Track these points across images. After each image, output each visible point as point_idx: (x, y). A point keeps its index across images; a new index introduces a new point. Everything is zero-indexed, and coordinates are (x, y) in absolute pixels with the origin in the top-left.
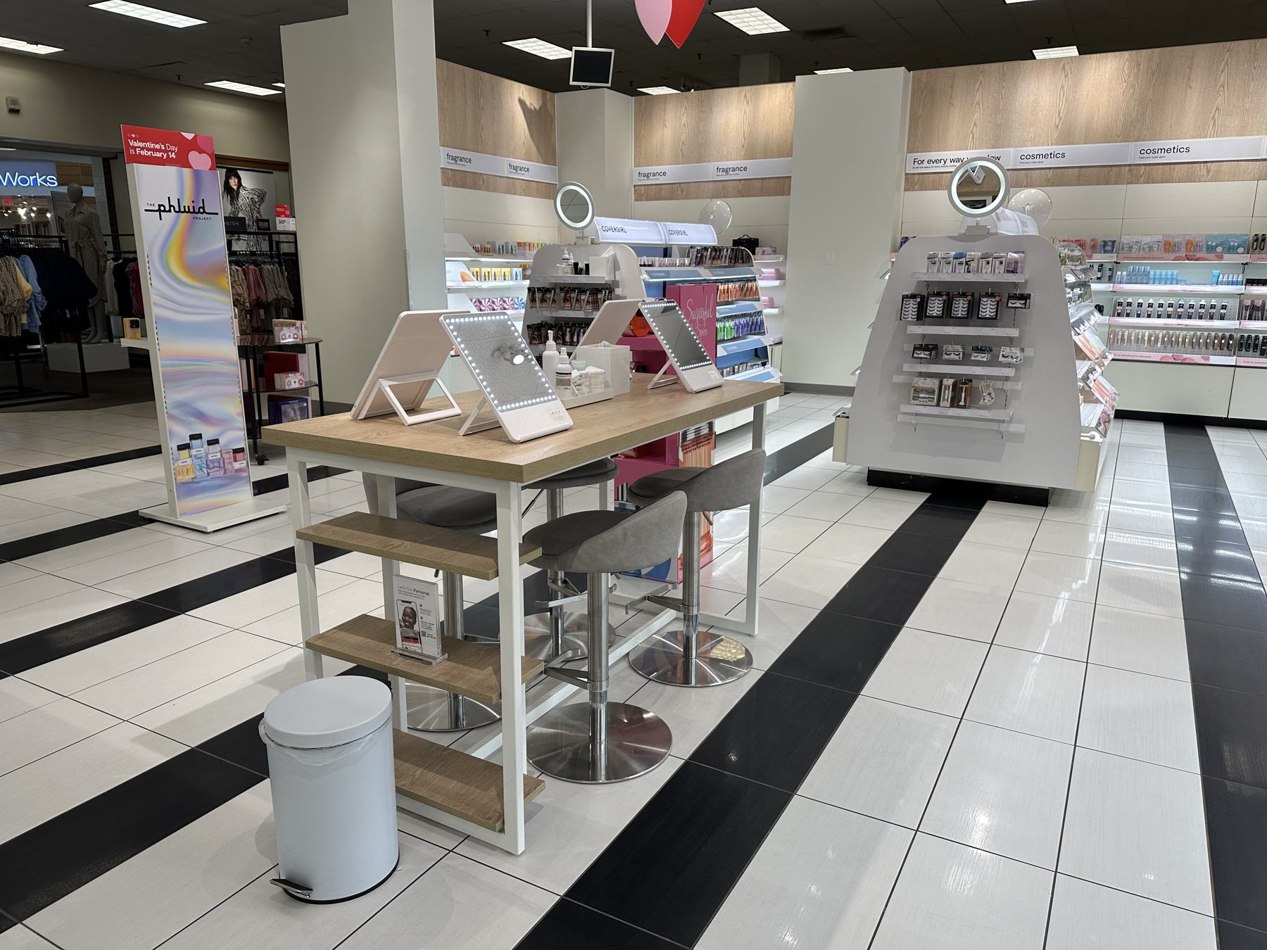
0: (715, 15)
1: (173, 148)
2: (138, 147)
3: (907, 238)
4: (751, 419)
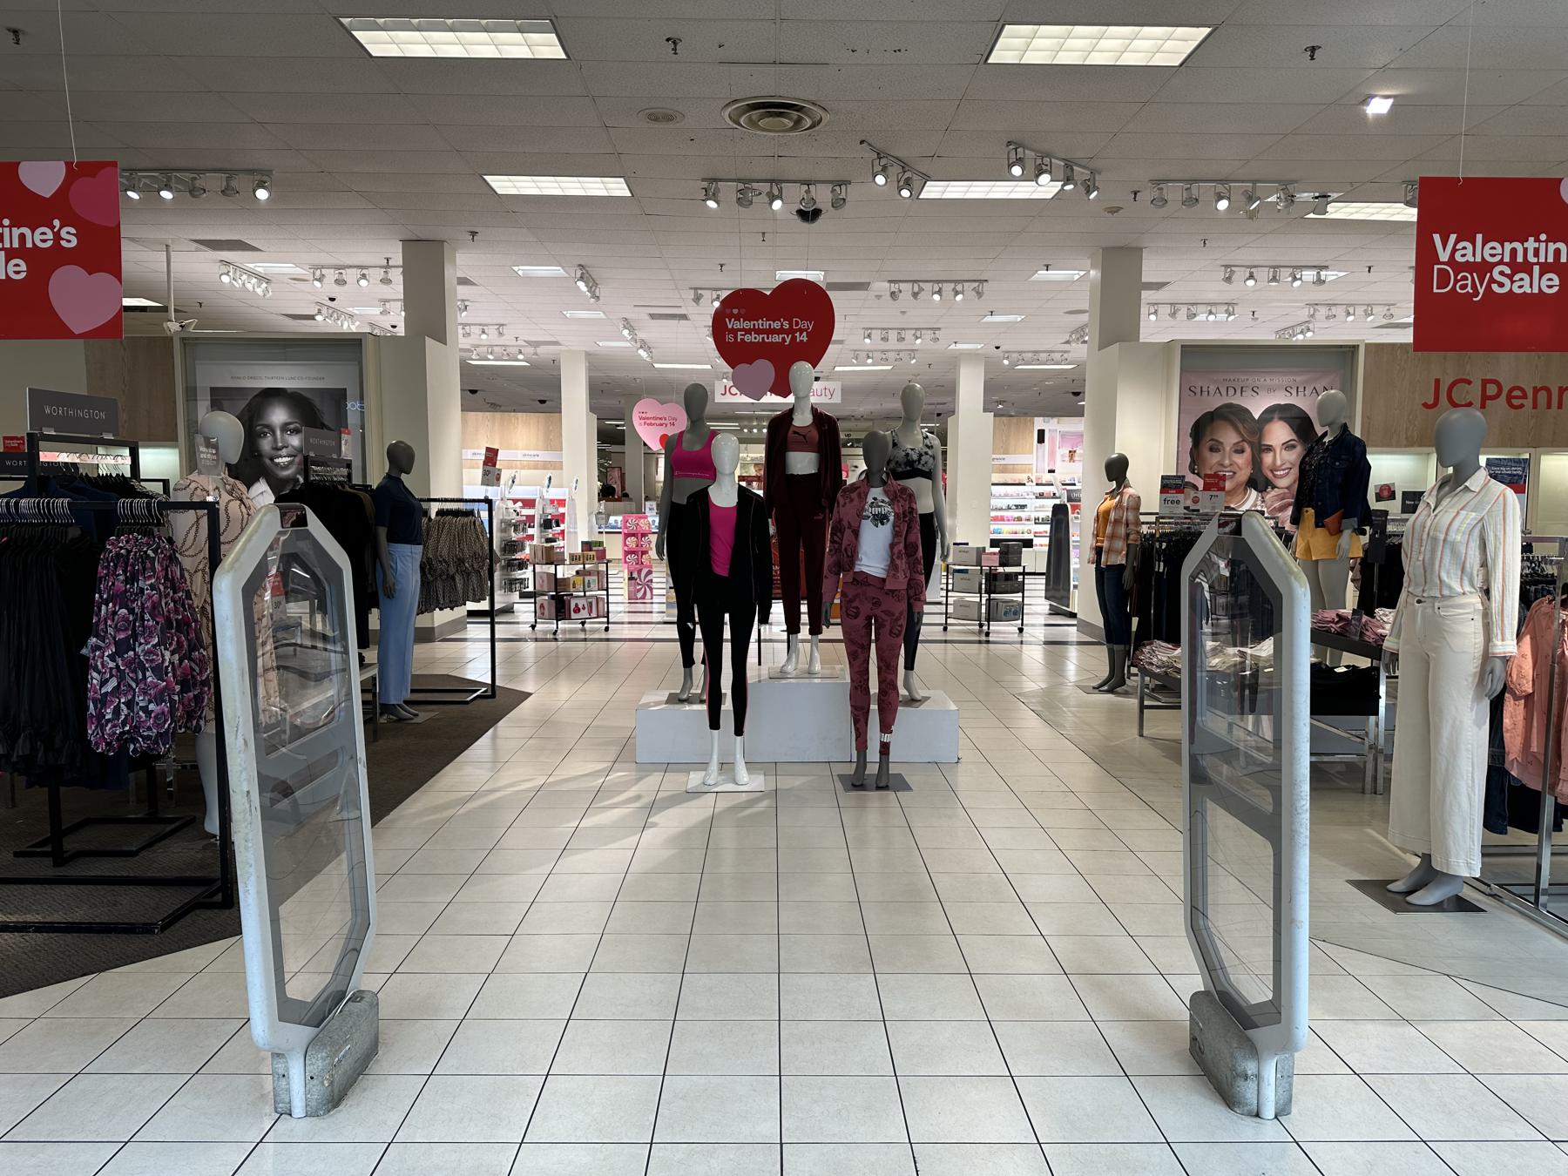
0: (484, 179)
1: (804, 324)
2: (740, 330)
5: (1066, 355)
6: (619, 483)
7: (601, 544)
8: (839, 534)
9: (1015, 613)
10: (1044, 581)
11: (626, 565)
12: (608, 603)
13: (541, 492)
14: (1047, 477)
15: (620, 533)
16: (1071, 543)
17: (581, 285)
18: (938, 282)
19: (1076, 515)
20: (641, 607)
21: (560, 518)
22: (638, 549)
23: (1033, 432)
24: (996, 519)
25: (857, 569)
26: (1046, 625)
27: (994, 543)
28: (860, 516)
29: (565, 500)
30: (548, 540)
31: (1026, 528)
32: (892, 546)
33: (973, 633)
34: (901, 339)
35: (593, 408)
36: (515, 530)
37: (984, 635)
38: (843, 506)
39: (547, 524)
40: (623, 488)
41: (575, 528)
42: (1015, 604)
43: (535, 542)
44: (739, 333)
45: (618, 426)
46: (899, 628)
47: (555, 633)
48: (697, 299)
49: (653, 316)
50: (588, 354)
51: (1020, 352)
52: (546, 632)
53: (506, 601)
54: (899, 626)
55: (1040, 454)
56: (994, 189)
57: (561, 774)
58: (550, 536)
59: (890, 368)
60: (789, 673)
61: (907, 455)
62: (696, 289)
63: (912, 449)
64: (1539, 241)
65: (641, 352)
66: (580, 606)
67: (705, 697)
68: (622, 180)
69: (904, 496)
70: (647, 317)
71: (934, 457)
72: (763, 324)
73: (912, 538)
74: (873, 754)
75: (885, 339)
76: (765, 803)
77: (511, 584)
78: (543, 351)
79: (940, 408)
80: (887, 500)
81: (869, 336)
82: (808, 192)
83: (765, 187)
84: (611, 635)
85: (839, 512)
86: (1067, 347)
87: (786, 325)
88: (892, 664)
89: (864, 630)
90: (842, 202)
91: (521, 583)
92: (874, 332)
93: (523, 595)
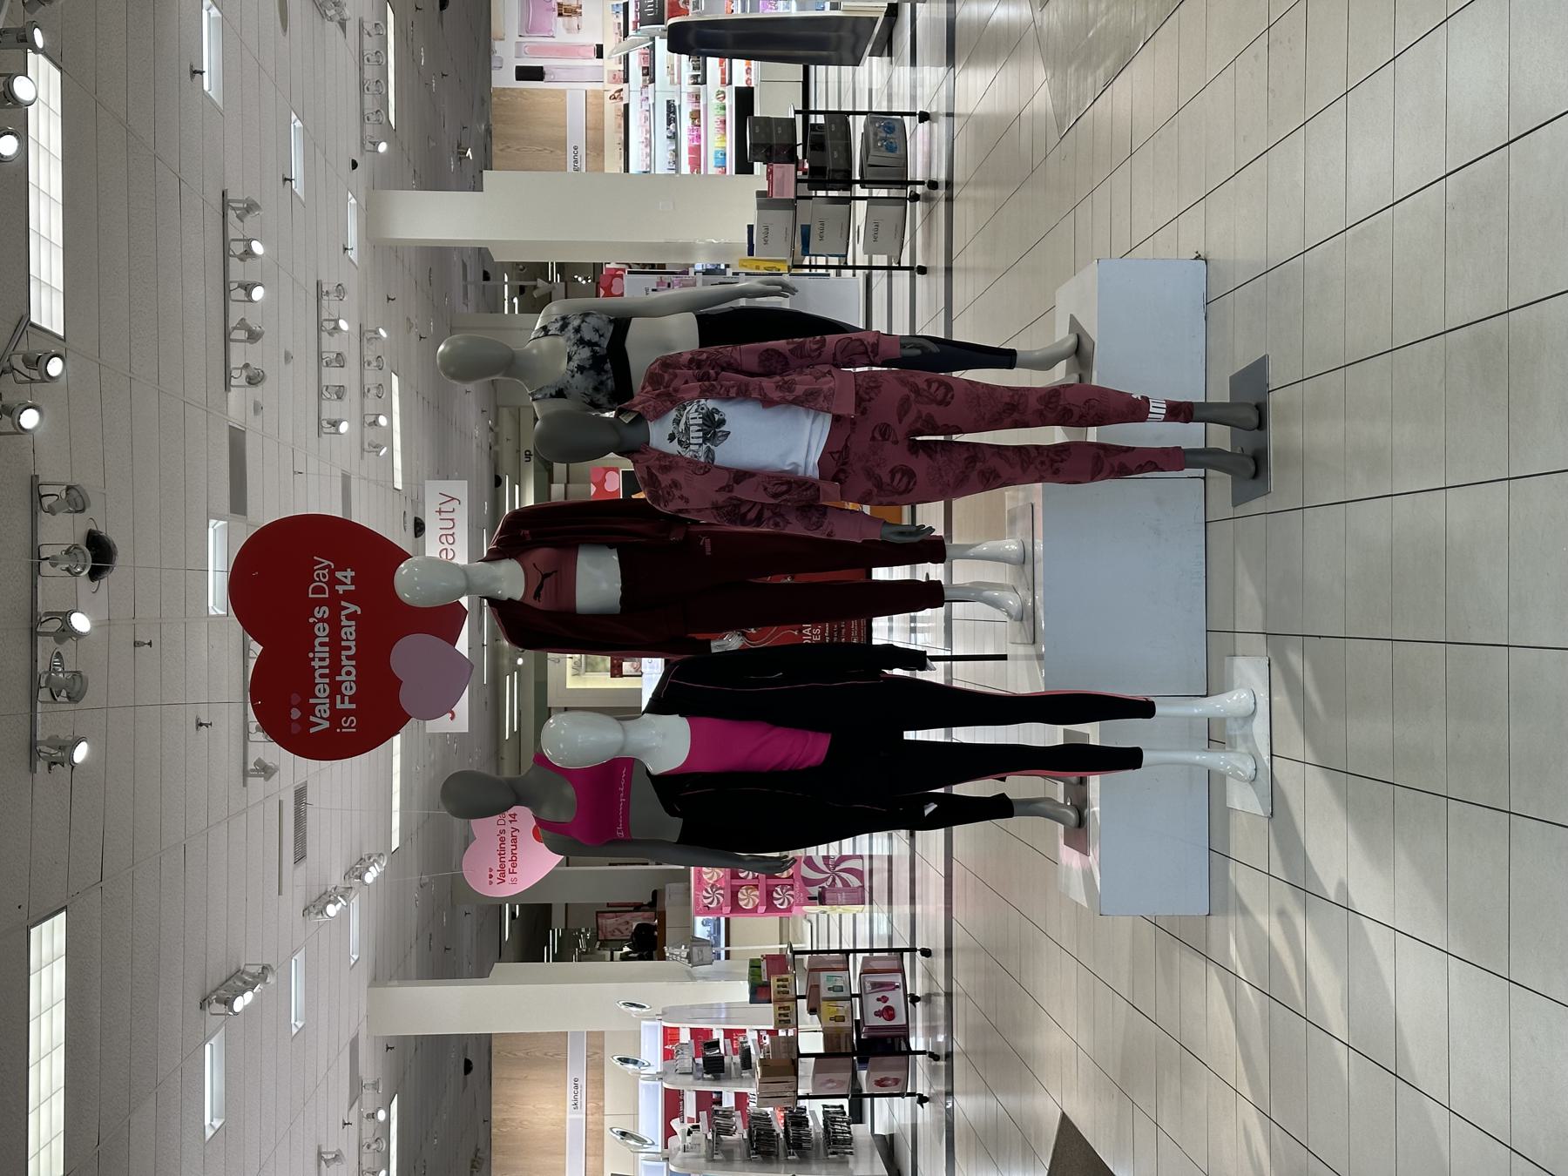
1: (320, 575)
3: (242, 319)
4: (1063, 826)
5: (368, 27)
6: (627, 917)
7: (755, 965)
8: (743, 509)
9: (890, 129)
10: (821, 69)
11: (795, 908)
12: (871, 951)
13: (652, 1077)
14: (611, 64)
15: (727, 921)
16: (749, 15)
17: (239, 1004)
18: (226, 291)
19: (690, 7)
20: (880, 880)
21: (702, 1040)
22: (762, 886)
23: (521, 91)
24: (696, 163)
25: (813, 472)
26: (913, 62)
27: (744, 167)
28: (708, 467)
29: (665, 1028)
30: (746, 1063)
31: (714, 102)
32: (767, 403)
33: (929, 215)
34: (340, 360)
35: (481, 972)
36: (728, 1133)
37: (934, 192)
38: (687, 501)
39: (715, 1067)
40: (638, 907)
41: (719, 1007)
42: (871, 129)
43: (752, 1090)
44: (339, 706)
45: (513, 915)
46: (934, 386)
47: (934, 1057)
48: (266, 771)
49: (300, 856)
50: (375, 981)
51: (363, 118)
52: (933, 1072)
53: (868, 1150)
54: (930, 387)
55: (564, 75)
56: (43, 141)
57: (1234, 1069)
58: (737, 1059)
59: (395, 379)
60: (1024, 604)
61: (581, 369)
62: (246, 774)
63: (570, 359)
64: (314, 657)
65: (369, 878)
66: (881, 1006)
67: (1074, 777)
68: (33, 931)
69: (667, 377)
70: (302, 866)
71: (586, 315)
72: (320, 657)
73: (751, 362)
74: (1190, 435)
75: (340, 392)
76: (1295, 659)
77: (836, 1141)
78: (370, 1069)
79: (474, 275)
80: (673, 414)
81: (335, 424)
82: (54, 561)
83: (46, 646)
84: (939, 945)
85: (699, 510)
86: (352, 27)
87: (322, 612)
88: (1008, 400)
89: (938, 456)
90: (73, 492)
91: (834, 1121)
92: (325, 416)
93: (857, 1116)
